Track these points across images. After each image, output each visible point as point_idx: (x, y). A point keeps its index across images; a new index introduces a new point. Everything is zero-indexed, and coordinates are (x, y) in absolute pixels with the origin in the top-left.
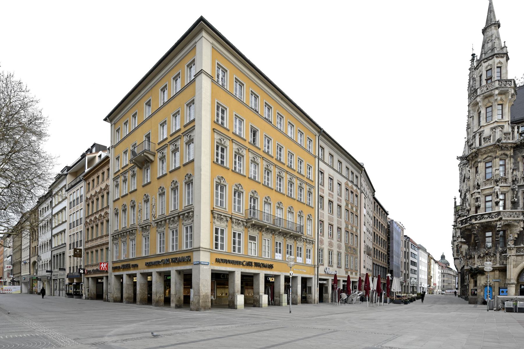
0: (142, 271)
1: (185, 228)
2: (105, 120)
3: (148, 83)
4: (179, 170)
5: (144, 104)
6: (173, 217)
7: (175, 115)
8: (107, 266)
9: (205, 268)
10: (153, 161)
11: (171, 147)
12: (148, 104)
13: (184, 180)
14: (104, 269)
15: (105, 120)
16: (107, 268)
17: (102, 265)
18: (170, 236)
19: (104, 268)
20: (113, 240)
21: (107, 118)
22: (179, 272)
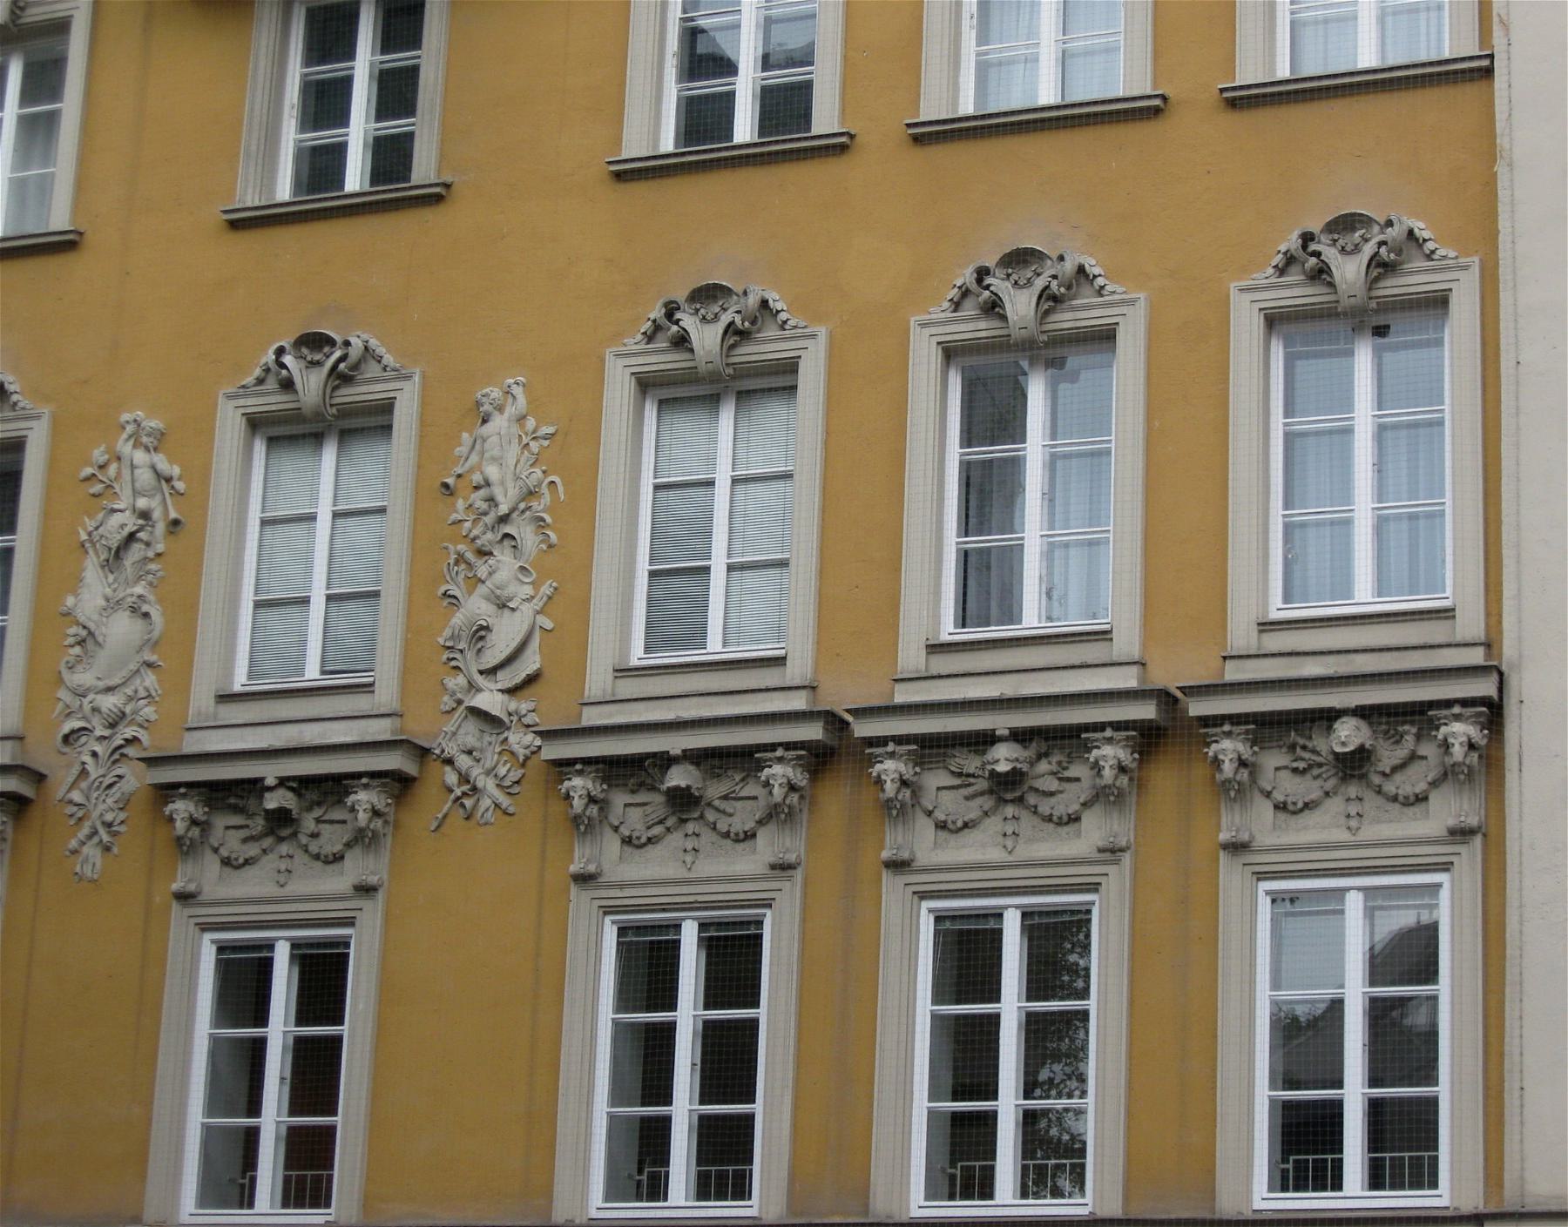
6: (302, 785)
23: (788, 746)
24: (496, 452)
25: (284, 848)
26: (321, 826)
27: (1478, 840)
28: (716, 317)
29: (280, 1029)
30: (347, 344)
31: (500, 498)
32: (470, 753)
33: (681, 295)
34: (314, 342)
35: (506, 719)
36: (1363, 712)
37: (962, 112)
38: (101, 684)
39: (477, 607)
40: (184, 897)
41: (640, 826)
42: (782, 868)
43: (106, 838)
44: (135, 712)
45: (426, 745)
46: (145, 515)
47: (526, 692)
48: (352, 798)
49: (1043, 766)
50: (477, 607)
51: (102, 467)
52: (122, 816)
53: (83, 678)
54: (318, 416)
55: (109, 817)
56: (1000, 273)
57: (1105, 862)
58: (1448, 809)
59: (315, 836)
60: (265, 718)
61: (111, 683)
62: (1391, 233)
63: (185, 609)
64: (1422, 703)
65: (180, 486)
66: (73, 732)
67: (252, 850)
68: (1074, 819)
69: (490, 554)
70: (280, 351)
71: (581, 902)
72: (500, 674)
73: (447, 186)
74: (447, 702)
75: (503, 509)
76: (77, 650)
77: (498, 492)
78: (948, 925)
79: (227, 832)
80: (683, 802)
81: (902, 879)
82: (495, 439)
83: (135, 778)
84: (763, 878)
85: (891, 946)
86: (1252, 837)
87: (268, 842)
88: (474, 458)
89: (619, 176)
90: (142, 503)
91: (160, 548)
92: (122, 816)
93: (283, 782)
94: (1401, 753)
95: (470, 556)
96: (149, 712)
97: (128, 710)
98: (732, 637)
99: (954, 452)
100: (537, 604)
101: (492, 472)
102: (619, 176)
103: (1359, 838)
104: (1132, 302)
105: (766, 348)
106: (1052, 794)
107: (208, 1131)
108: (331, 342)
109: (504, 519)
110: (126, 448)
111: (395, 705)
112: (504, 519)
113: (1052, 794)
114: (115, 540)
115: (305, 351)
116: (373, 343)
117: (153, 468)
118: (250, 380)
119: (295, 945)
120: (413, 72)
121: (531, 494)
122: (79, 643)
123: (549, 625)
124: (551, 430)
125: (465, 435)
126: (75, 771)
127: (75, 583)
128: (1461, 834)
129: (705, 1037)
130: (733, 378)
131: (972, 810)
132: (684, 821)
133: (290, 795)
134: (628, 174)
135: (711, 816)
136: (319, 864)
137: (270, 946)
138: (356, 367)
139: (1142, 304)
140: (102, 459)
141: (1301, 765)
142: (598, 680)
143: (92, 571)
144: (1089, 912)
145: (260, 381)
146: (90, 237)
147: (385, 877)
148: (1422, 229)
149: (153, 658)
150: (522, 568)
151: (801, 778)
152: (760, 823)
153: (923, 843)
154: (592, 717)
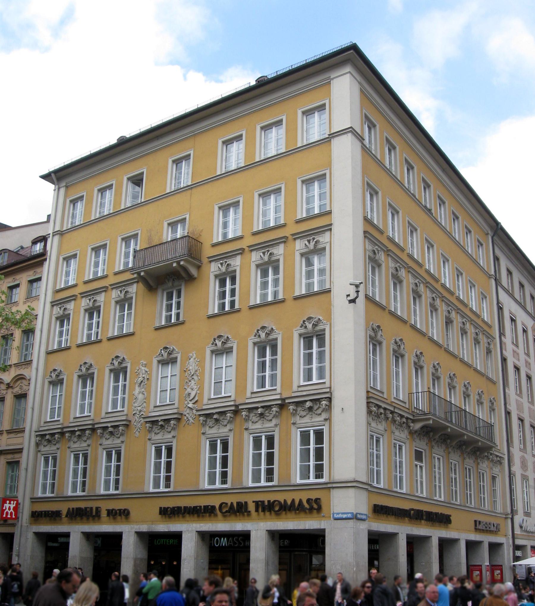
0: (144, 528)
1: (43, 458)
2: (46, 177)
3: (197, 120)
4: (280, 305)
5: (93, 190)
6: (164, 420)
7: (96, 250)
8: (16, 509)
9: (361, 527)
10: (195, 279)
11: (85, 303)
12: (137, 181)
13: (48, 377)
14: (9, 516)
15: (46, 177)
16: (16, 515)
17: (7, 505)
18: (40, 467)
19: (9, 512)
20: (37, 445)
21: (53, 175)
22: (202, 535)
23: (230, 410)
24: (191, 364)
25: (163, 431)
26: (168, 427)
27: (328, 421)
28: (311, 323)
29: (264, 451)
30: (170, 348)
31: (192, 372)
32: (188, 414)
33: (216, 337)
34: (166, 348)
35: (193, 408)
36: (311, 400)
37: (257, 303)
38: (138, 406)
39: (189, 390)
40: (246, 429)
41: (211, 425)
42: (230, 430)
43: (139, 430)
44: (143, 410)
45: (182, 413)
46: (144, 378)
47: (196, 403)
48: (322, 403)
49: (267, 412)
50: (189, 390)
51: (138, 370)
52: (141, 427)
53: (136, 405)
54: (167, 360)
55: (139, 427)
56: (307, 321)
57: (276, 427)
58: (324, 416)
59: (167, 428)
60: (165, 409)
61: (139, 405)
62: (316, 319)
63: (149, 393)
64: (270, 405)
65: (148, 372)
66: (134, 413)
67: (159, 431)
68: (320, 414)
69: (191, 381)
70: (161, 350)
71: (203, 438)
72: (192, 401)
73: (184, 321)
74: (185, 406)
75: (192, 374)
76: (135, 400)
77: (191, 371)
78: (255, 438)
79: (210, 422)
80: (217, 420)
81: (204, 436)
82: (191, 362)
83: (143, 421)
84: (228, 432)
85: (246, 442)
86: (296, 422)
87: (161, 430)
88: (189, 365)
89: (208, 318)
90: (143, 376)
91: (146, 383)
92: (141, 427)
93: (161, 420)
94: (317, 407)
95: (188, 382)
96: (145, 410)
97: (142, 409)
98: (226, 393)
99: (256, 359)
100: (197, 389)
101: (191, 368)
102: (208, 318)
103: (312, 421)
104: (279, 334)
105: (228, 345)
106: (268, 416)
107: (253, 469)
108: (168, 348)
109: (193, 375)
110: (141, 367)
111: (280, 392)
112: (193, 375)
113: (268, 416)
114: (140, 382)
115: (165, 350)
116: (174, 347)
117: (145, 370)
118: (158, 355)
119: (266, 436)
120: (235, 289)
121: (196, 371)
122: (135, 399)
123: (199, 392)
124: (199, 360)
125: (187, 362)
126: (135, 420)
127: (134, 389)
128: (326, 420)
129: (316, 450)
130: (225, 350)
131: (159, 431)
132: (217, 423)
133: (163, 422)
134: (210, 317)
135: (221, 422)
136: (268, 422)
137: (162, 446)
138: (172, 352)
139: (281, 334)
140: (138, 369)
141: (303, 409)
142: (205, 401)
143: (137, 387)
144: (323, 430)
145: (159, 355)
146: (136, 333)
147: (177, 434)
148: (321, 318)
149: (145, 401)
150: (195, 383)
151: (232, 416)
152: (272, 418)
153: (251, 426)
154: (204, 407)
